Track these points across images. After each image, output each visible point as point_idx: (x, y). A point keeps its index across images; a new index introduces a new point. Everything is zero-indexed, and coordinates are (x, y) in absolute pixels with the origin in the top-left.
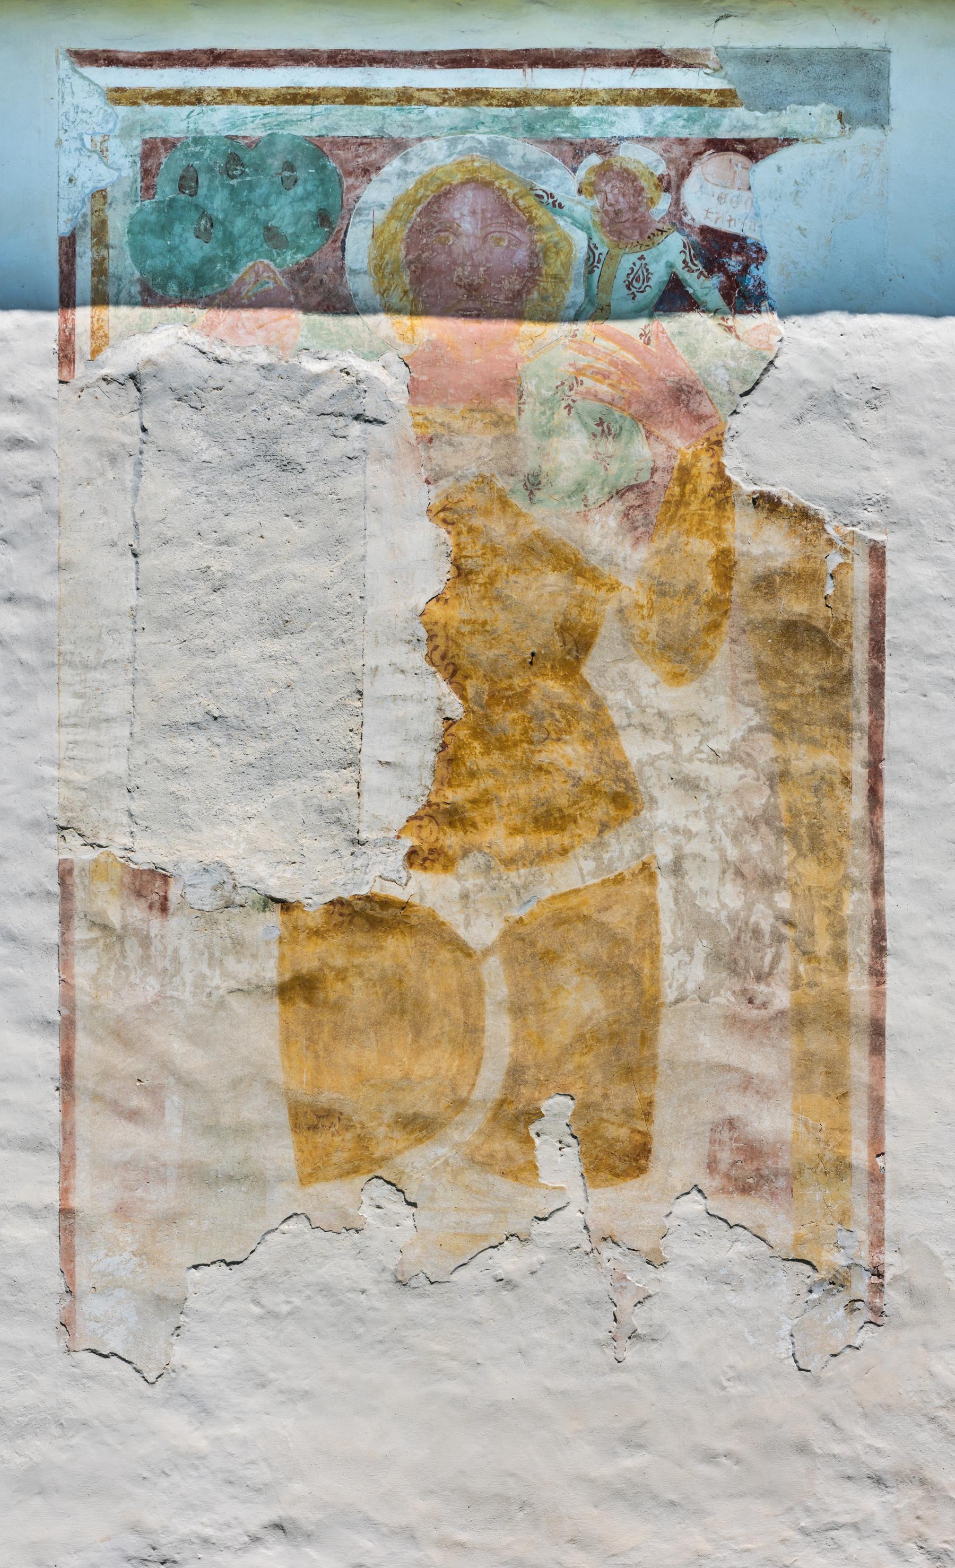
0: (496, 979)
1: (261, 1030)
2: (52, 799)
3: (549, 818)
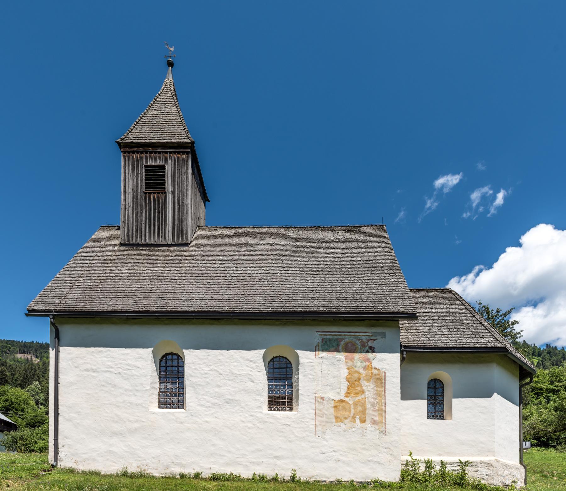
0: (352, 407)
1: (332, 410)
2: (314, 391)
3: (357, 393)
